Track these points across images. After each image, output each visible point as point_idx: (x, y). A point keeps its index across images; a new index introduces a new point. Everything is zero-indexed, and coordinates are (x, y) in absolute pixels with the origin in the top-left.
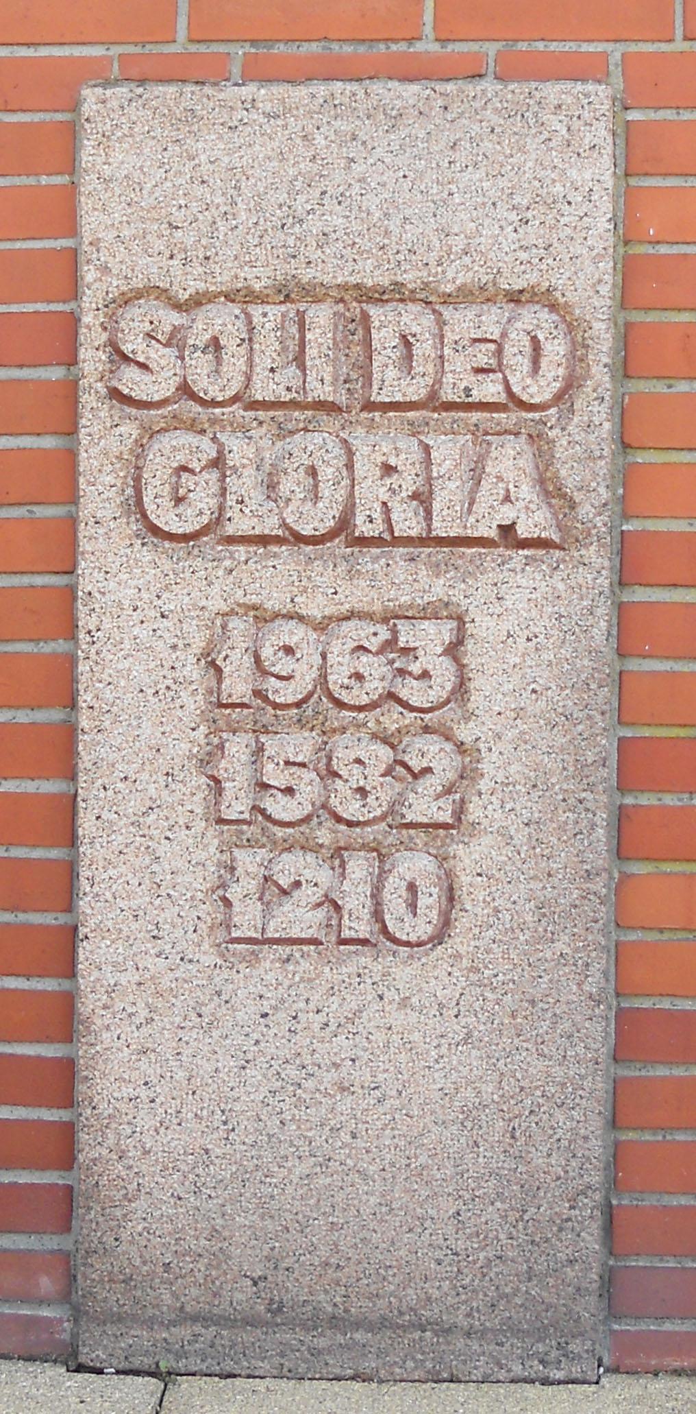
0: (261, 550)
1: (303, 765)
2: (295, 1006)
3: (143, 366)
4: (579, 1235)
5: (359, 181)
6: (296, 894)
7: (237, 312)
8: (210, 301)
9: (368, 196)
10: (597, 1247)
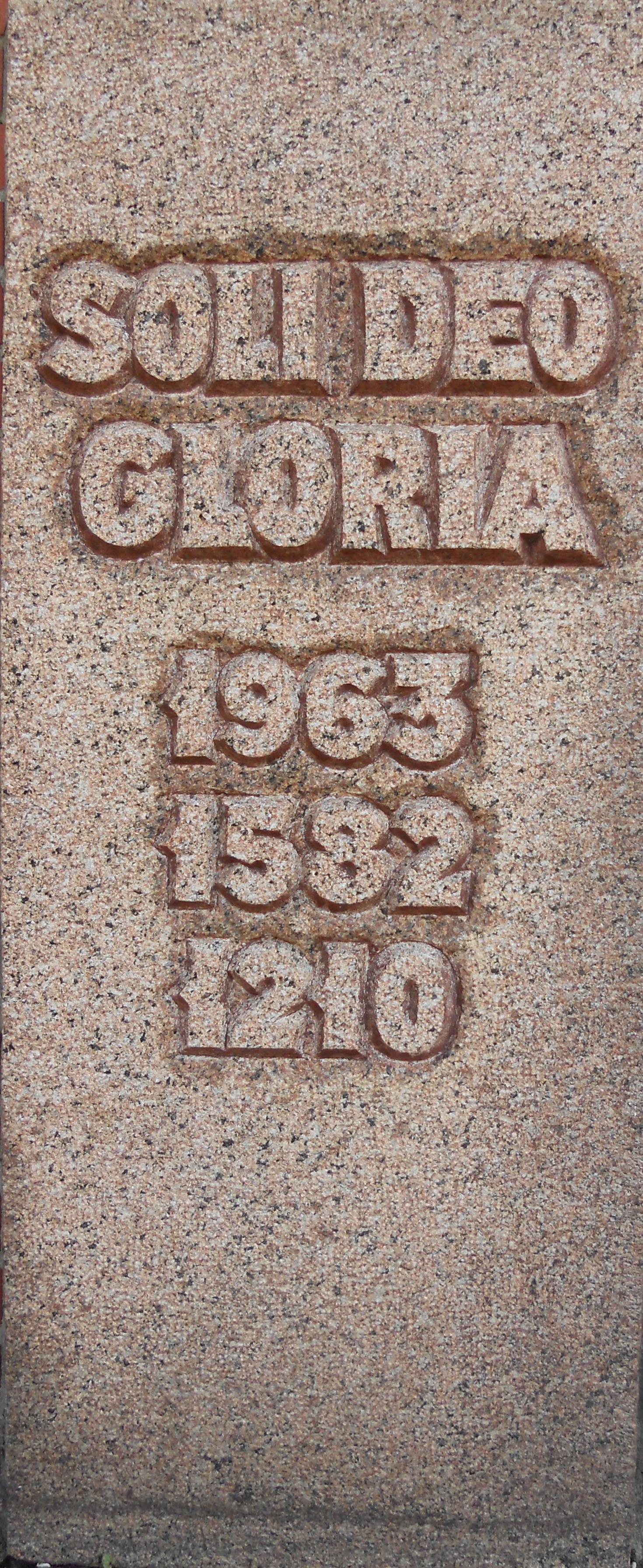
0: (226, 568)
1: (276, 834)
2: (266, 1133)
3: (83, 341)
4: (611, 1411)
5: (350, 107)
6: (267, 994)
7: (198, 273)
8: (165, 261)
9: (361, 126)
10: (634, 1426)
